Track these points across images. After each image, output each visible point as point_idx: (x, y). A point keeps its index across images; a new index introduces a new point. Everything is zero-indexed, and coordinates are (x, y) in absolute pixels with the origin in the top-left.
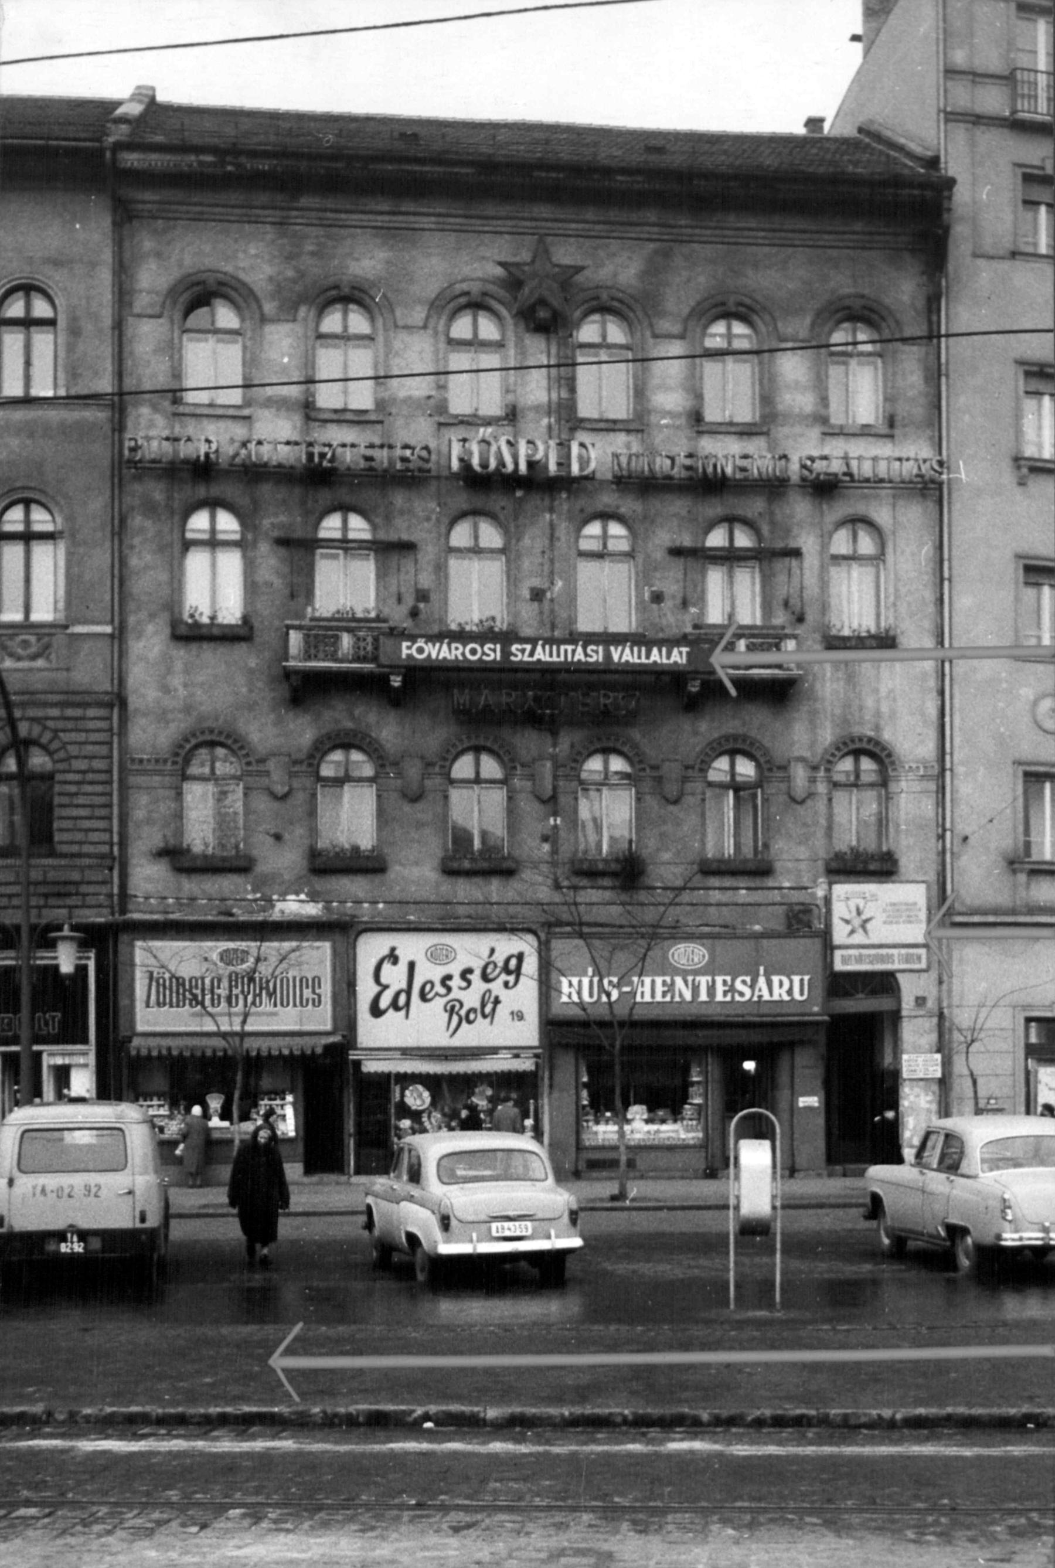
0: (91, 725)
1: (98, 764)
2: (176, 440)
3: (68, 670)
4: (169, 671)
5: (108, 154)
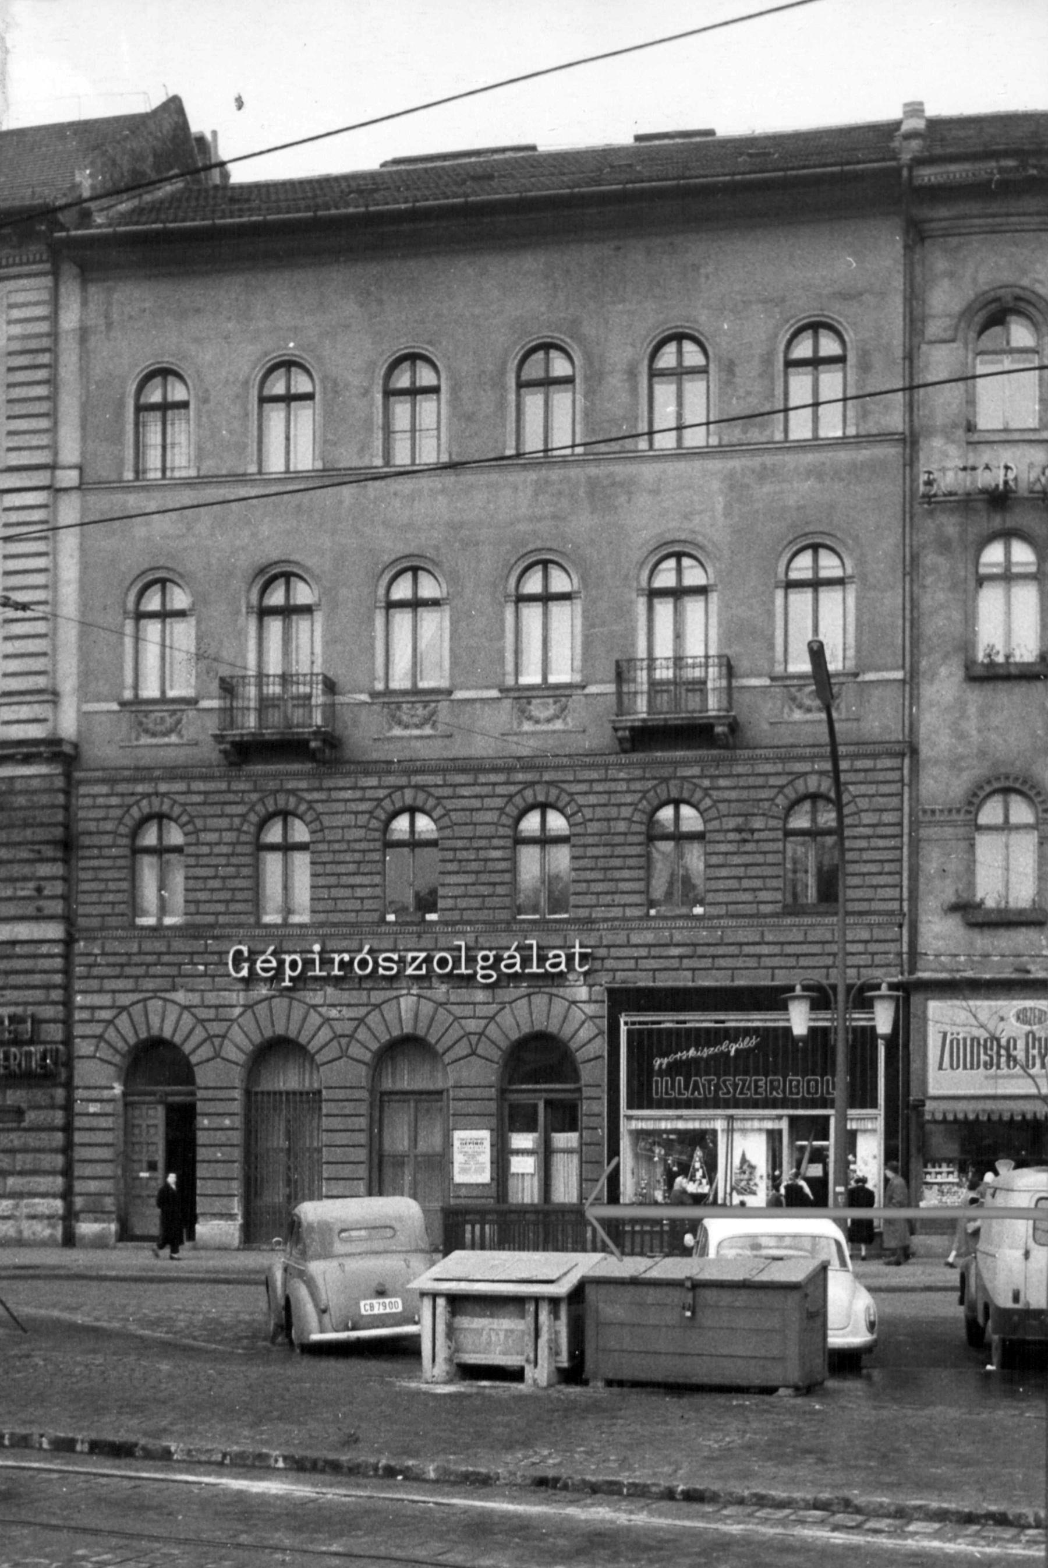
0: (881, 776)
1: (888, 818)
2: (974, 469)
3: (858, 720)
4: (963, 715)
5: (905, 173)
